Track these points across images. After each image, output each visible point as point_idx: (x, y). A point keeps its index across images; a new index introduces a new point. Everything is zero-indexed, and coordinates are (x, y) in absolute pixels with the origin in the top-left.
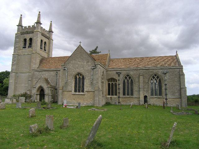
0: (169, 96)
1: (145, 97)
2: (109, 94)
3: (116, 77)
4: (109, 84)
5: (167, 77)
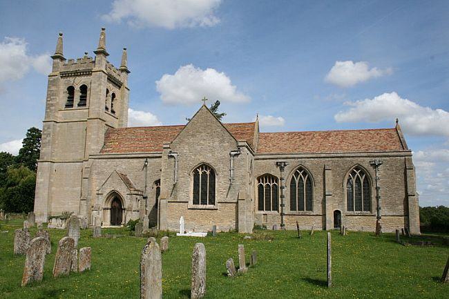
0: (383, 212)
1: (337, 213)
2: (261, 208)
3: (275, 172)
4: (261, 187)
5: (380, 173)
